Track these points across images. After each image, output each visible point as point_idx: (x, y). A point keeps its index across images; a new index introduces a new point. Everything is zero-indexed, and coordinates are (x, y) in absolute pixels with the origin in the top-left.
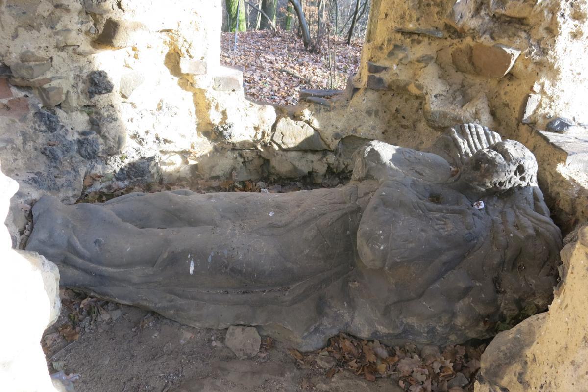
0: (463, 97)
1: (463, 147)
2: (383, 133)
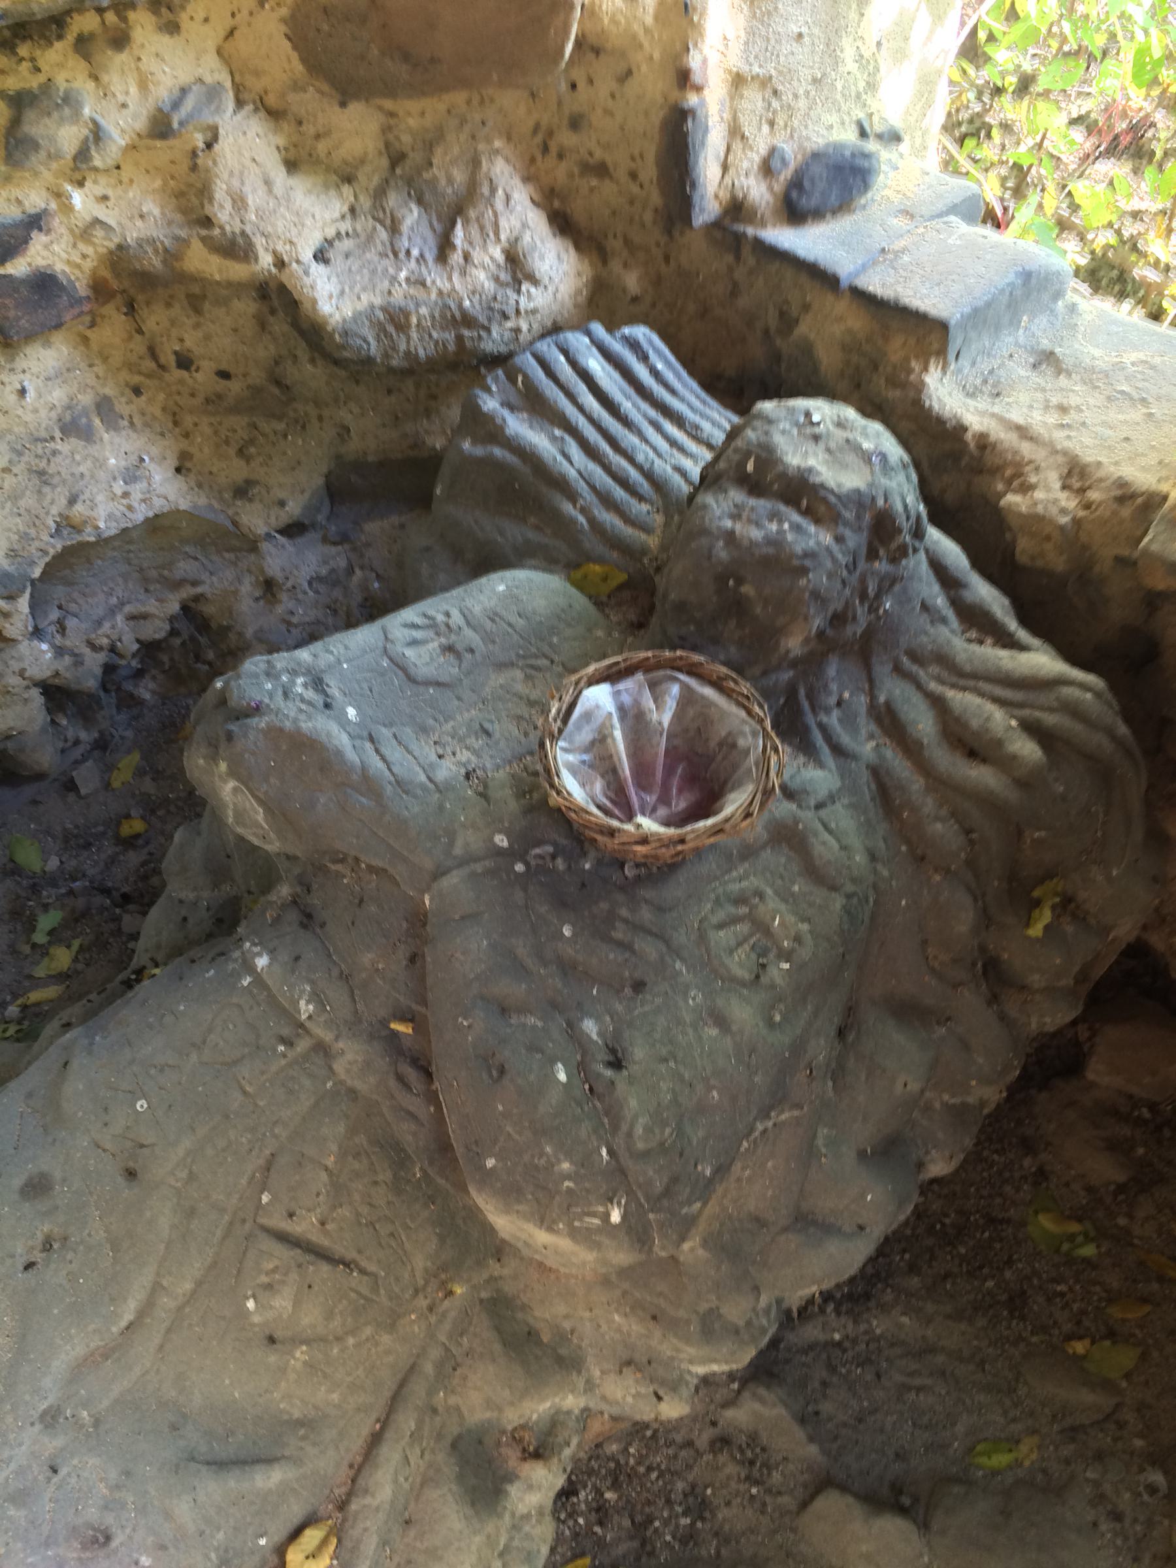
0: (420, 202)
1: (572, 473)
2: (178, 470)
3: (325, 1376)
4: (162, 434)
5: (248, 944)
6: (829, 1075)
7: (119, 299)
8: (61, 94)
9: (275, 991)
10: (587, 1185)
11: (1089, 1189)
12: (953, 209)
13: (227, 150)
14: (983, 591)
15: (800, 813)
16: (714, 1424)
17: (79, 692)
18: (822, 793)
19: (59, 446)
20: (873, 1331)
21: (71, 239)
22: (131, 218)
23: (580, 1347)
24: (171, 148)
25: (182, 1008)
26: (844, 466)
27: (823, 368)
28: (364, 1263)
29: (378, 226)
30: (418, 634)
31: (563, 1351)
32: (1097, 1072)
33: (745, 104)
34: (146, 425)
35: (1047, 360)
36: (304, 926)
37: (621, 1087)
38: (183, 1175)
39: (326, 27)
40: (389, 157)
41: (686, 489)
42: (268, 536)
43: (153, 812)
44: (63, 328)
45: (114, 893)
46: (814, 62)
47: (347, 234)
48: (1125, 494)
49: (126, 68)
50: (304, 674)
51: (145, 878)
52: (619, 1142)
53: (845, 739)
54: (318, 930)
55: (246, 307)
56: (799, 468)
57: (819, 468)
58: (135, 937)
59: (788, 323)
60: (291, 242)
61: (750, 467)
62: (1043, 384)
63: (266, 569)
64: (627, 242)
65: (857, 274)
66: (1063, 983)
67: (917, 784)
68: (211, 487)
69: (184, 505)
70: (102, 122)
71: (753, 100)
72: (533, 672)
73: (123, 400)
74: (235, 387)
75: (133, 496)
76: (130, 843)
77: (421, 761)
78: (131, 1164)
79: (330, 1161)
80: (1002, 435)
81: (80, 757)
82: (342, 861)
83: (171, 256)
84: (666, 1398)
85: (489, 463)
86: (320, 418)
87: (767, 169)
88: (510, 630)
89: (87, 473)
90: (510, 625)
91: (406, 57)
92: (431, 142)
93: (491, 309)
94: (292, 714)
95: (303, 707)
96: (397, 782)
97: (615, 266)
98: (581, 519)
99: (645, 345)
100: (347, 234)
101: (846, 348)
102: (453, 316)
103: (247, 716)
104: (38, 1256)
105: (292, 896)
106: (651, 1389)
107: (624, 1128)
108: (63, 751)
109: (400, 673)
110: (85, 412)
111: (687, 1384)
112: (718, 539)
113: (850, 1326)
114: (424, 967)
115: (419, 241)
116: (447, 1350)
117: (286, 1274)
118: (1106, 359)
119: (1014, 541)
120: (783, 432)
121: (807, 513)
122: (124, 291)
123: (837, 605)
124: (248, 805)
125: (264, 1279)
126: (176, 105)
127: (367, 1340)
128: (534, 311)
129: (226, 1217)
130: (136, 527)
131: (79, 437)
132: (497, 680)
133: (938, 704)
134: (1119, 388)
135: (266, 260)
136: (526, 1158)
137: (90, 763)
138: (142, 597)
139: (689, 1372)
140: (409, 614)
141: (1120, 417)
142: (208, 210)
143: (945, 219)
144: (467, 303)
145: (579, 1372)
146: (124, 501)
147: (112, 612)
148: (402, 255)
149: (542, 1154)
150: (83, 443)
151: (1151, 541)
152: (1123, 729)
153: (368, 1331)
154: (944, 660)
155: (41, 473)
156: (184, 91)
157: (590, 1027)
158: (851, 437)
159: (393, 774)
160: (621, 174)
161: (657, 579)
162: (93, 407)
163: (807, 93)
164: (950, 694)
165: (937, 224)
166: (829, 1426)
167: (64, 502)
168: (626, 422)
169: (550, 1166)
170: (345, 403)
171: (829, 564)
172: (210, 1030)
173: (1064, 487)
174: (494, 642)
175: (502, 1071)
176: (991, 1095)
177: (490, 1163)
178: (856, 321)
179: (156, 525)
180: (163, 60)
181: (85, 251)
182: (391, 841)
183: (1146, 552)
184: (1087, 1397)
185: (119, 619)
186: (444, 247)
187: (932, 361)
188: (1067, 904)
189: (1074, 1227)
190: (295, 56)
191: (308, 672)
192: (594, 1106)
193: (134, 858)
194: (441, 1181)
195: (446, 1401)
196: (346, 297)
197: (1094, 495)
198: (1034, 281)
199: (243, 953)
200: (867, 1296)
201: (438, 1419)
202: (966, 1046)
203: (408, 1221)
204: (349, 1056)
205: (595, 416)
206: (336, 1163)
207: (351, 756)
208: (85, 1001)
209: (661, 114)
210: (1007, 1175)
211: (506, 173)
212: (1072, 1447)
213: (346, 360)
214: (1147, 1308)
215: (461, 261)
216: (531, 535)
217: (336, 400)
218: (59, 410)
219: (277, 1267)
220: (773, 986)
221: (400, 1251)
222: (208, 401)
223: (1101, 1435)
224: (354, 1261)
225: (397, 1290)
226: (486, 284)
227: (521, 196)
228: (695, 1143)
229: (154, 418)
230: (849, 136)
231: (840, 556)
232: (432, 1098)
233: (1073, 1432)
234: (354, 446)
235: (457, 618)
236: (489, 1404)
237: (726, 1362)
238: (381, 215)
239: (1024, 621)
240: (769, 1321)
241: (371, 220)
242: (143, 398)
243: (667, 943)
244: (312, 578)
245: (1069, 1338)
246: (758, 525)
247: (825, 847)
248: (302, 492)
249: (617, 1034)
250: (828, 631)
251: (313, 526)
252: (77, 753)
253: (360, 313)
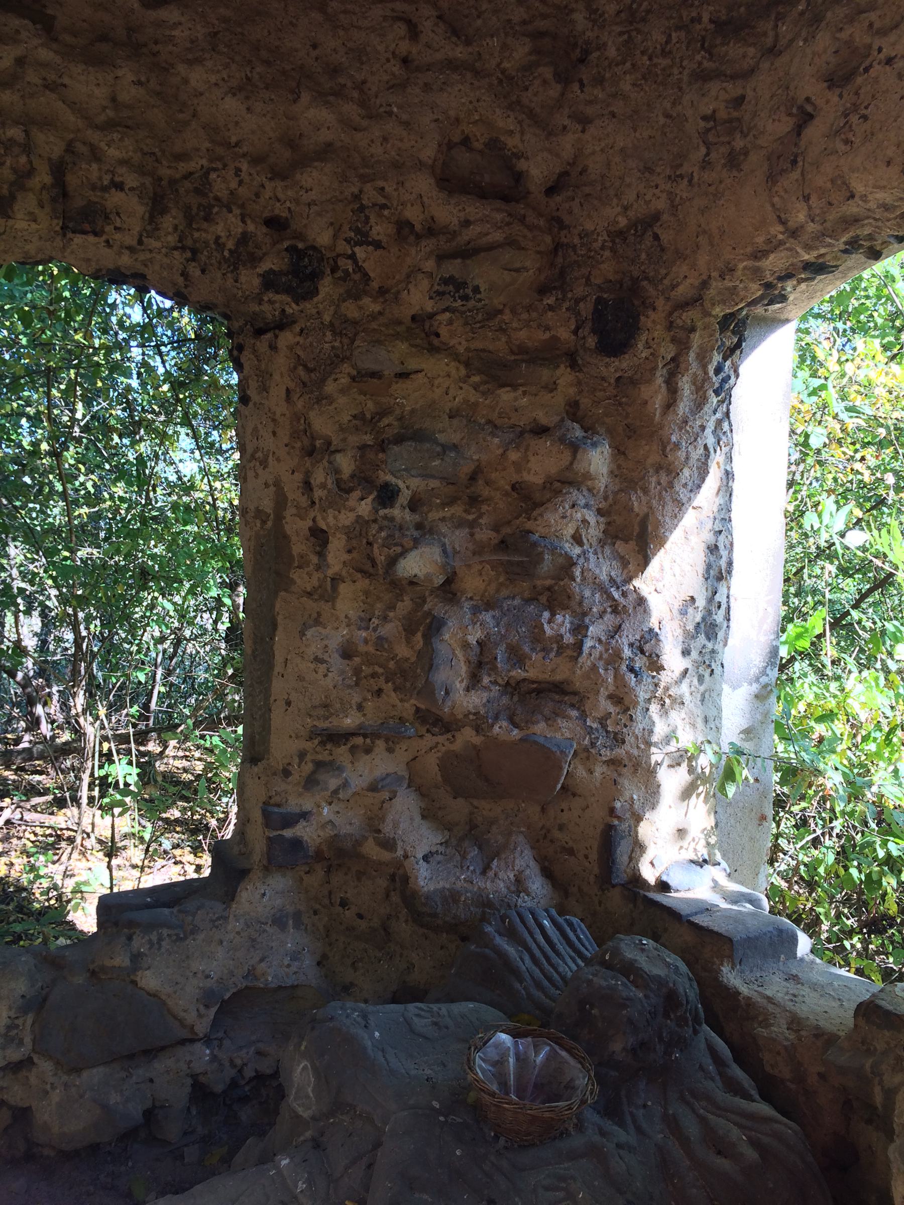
2: (319, 964)
14: (737, 1072)
19: (267, 928)
48: (819, 1033)
74: (363, 925)
83: (358, 843)
133: (703, 1120)
135: (400, 853)
155: (254, 940)
164: (711, 1117)
197: (803, 1033)
227: (528, 854)
246: (606, 980)
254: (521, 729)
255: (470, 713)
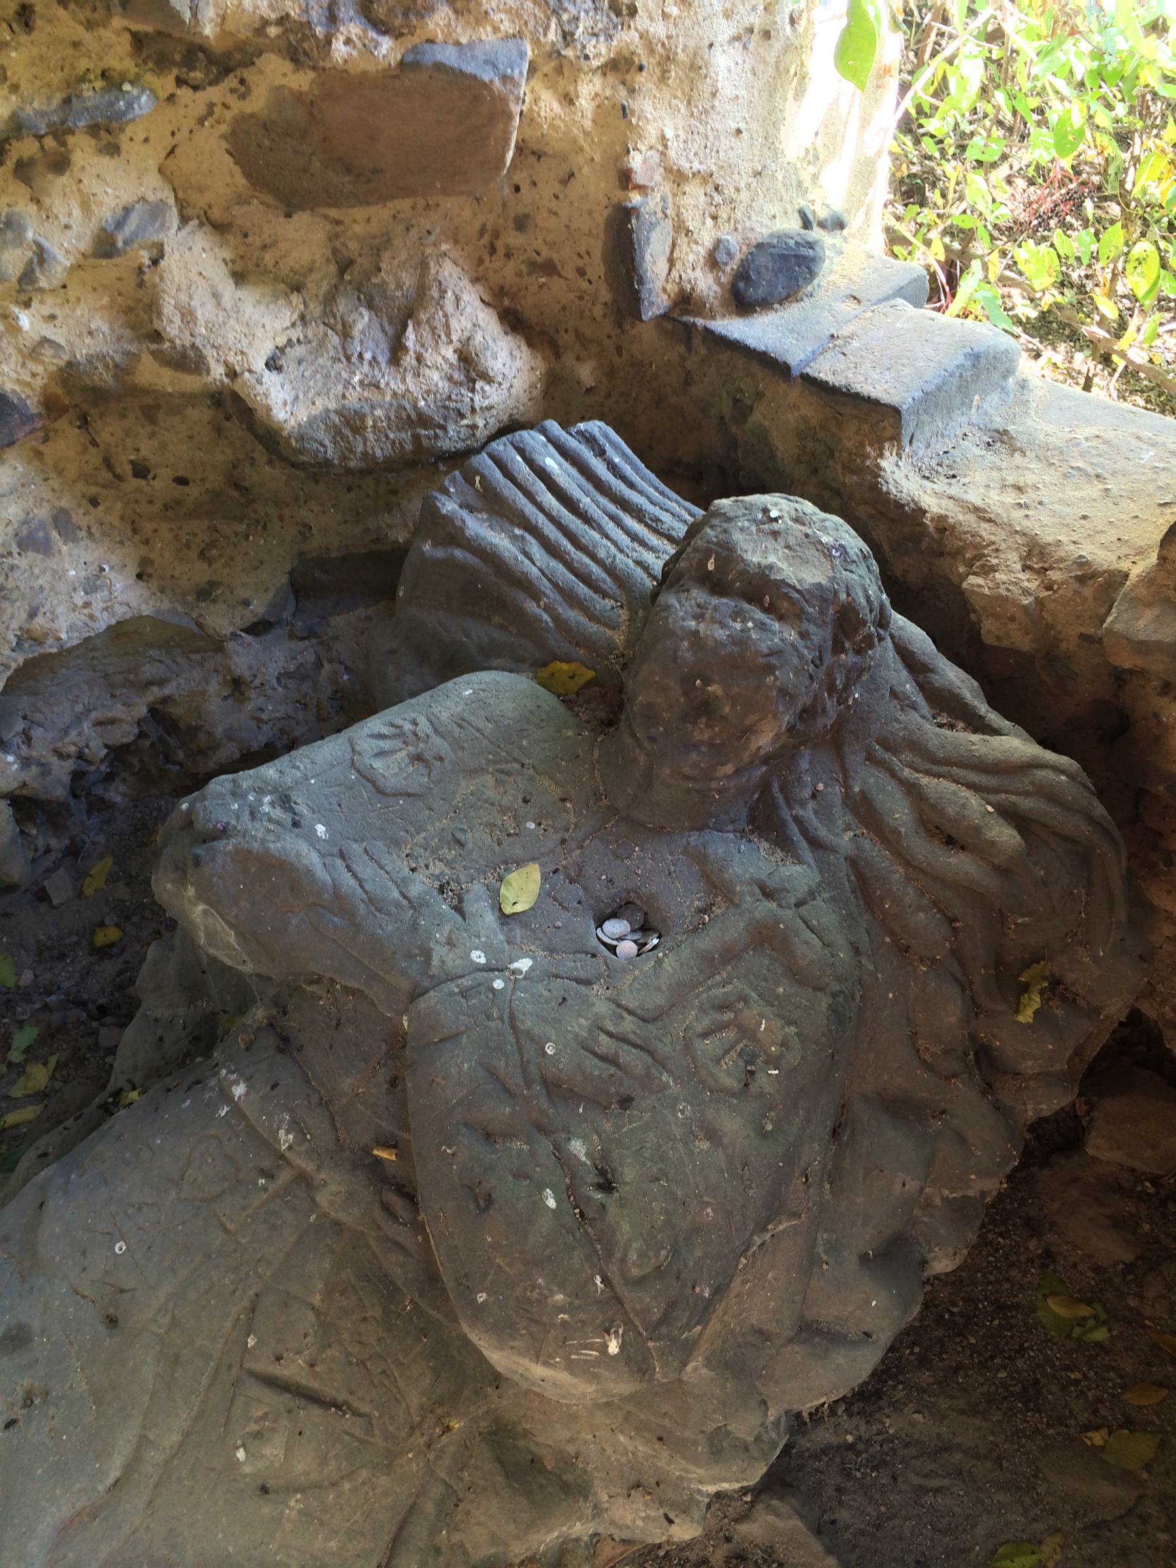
0: (370, 306)
1: (535, 571)
2: (139, 576)
3: (322, 1523)
4: (122, 543)
5: (224, 1071)
6: (826, 1177)
7: (72, 414)
8: (3, 219)
9: (253, 1122)
10: (582, 1316)
11: (1097, 1270)
12: (900, 292)
13: (174, 267)
14: (951, 675)
15: (780, 911)
16: (728, 1539)
17: (48, 802)
18: (802, 891)
19: (17, 560)
20: (887, 1432)
21: (20, 359)
22: (80, 336)
23: (586, 1472)
24: (116, 265)
25: (159, 1141)
26: (805, 562)
27: (779, 454)
28: (356, 1404)
29: (330, 332)
30: (386, 745)
31: (567, 1477)
32: (1097, 1146)
33: (687, 200)
34: (105, 534)
35: (1000, 439)
36: (280, 1050)
37: (612, 1210)
38: (166, 1320)
39: (267, 143)
40: (337, 263)
41: (649, 583)
42: (234, 636)
43: (128, 918)
44: (16, 445)
45: (90, 1006)
46: (753, 155)
47: (298, 340)
48: (1086, 574)
49: (67, 190)
50: (271, 793)
51: (121, 988)
52: (613, 1270)
53: (822, 832)
54: (295, 1054)
55: (201, 414)
56: (759, 565)
57: (780, 564)
58: (112, 1051)
59: (742, 411)
60: (242, 353)
61: (711, 566)
62: (999, 463)
63: (233, 667)
64: (579, 335)
65: (807, 363)
66: (1058, 1067)
67: (898, 873)
68: (173, 590)
69: (146, 610)
70: (46, 244)
71: (694, 195)
72: (503, 777)
73: (81, 511)
74: (193, 492)
75: (94, 605)
76: (104, 952)
77: (393, 875)
78: (111, 1310)
79: (317, 1300)
80: (961, 517)
81: (51, 865)
82: (317, 981)
83: (122, 371)
84: (676, 1521)
85: (450, 564)
86: (281, 518)
87: (713, 262)
88: (478, 735)
89: (47, 586)
90: (478, 730)
91: (348, 170)
92: (379, 246)
93: (446, 408)
94: (260, 835)
95: (271, 827)
96: (371, 901)
97: (568, 359)
98: (546, 617)
99: (602, 440)
100: (298, 340)
101: (800, 435)
102: (409, 416)
103: (214, 839)
104: (19, 1413)
105: (267, 1018)
106: (661, 1511)
107: (618, 1255)
108: (33, 860)
109: (368, 784)
110: (42, 526)
111: (698, 1503)
112: (683, 639)
113: (863, 1428)
114: (404, 1090)
115: (371, 344)
116: (447, 1485)
117: (275, 1421)
118: (1060, 435)
119: (980, 621)
120: (742, 530)
121: (769, 610)
122: (76, 405)
123: (804, 700)
124: (219, 929)
125: (253, 1427)
126: (120, 224)
127: (364, 1483)
128: (489, 408)
129: (212, 1364)
130: (98, 635)
131: (37, 551)
132: (466, 787)
133: (912, 790)
134: (1074, 465)
135: (218, 372)
136: (518, 1291)
137: (61, 872)
138: (109, 702)
139: (699, 1491)
140: (375, 724)
141: (1078, 494)
142: (157, 325)
143: (892, 302)
144: (422, 403)
145: (586, 1498)
146: (86, 611)
147: (78, 719)
148: (354, 359)
149: (534, 1287)
150: (41, 556)
151: (1112, 622)
152: (1100, 810)
153: (364, 1474)
154: (916, 746)
156: (127, 210)
157: (578, 1148)
158: (809, 531)
159: (365, 891)
160: (569, 272)
161: (624, 676)
162: (50, 520)
163: (749, 185)
164: (925, 780)
165: (884, 307)
166: (847, 1535)
167: (24, 615)
168: (586, 519)
169: (542, 1300)
170: (305, 502)
171: (795, 661)
172: (188, 1164)
173: (1025, 568)
174: (463, 748)
175: (489, 1200)
176: (993, 1185)
177: (482, 1297)
178: (810, 410)
179: (119, 632)
180: (105, 181)
181: (34, 370)
182: (366, 962)
183: (1110, 631)
184: (1107, 1491)
185: (86, 725)
186: (397, 350)
187: (887, 445)
188: (1056, 988)
189: (1084, 1311)
190: (237, 171)
191: (274, 790)
192: (586, 1231)
193: (109, 968)
194: (433, 1313)
195: (449, 1541)
196: (300, 402)
197: (1054, 575)
198: (983, 361)
199: (219, 1080)
200: (879, 1394)
201: (441, 1559)
202: (962, 1139)
203: (400, 1357)
204: (333, 1188)
205: (554, 513)
206: (322, 1300)
207: (321, 874)
208: (61, 1127)
209: (606, 212)
210: (1013, 1258)
211: (454, 275)
212: (1095, 1545)
213: (303, 463)
214: (1164, 1393)
215: (414, 362)
216: (497, 635)
217: (296, 499)
218: (16, 526)
219: (266, 1414)
220: (762, 1095)
221: (393, 1389)
222: (166, 507)
223: (1125, 1531)
224: (345, 1403)
225: (392, 1429)
226: (440, 385)
227: (471, 297)
228: (692, 1264)
229: (113, 527)
230: (793, 225)
231: (806, 652)
232: (419, 1228)
233: (1096, 1529)
234: (316, 543)
235: (424, 726)
236: (494, 1540)
237: (737, 1481)
238: (332, 321)
239: (992, 702)
240: (778, 1434)
241: (322, 326)
242: (100, 508)
243: (651, 1053)
244: (280, 674)
245: (1086, 1428)
246: (723, 625)
247: (807, 947)
248: (267, 590)
249: (605, 1155)
250: (798, 726)
251: (279, 622)
252: (48, 862)
253: (315, 417)
254: (398, 36)
255: (265, 23)
